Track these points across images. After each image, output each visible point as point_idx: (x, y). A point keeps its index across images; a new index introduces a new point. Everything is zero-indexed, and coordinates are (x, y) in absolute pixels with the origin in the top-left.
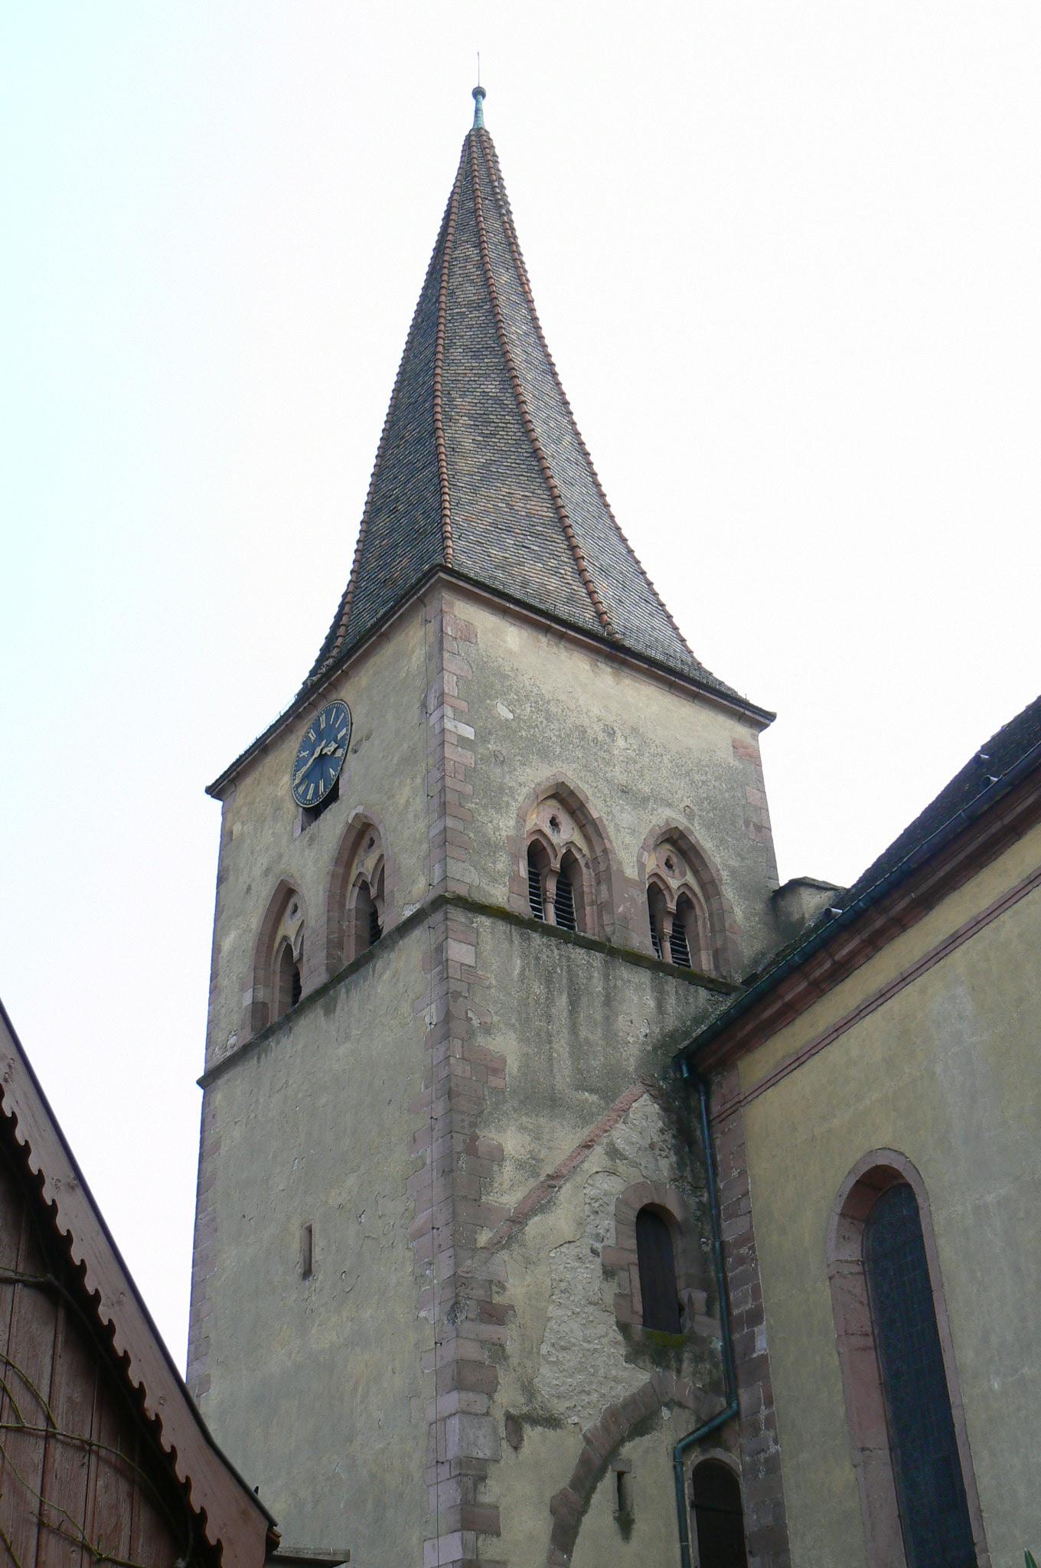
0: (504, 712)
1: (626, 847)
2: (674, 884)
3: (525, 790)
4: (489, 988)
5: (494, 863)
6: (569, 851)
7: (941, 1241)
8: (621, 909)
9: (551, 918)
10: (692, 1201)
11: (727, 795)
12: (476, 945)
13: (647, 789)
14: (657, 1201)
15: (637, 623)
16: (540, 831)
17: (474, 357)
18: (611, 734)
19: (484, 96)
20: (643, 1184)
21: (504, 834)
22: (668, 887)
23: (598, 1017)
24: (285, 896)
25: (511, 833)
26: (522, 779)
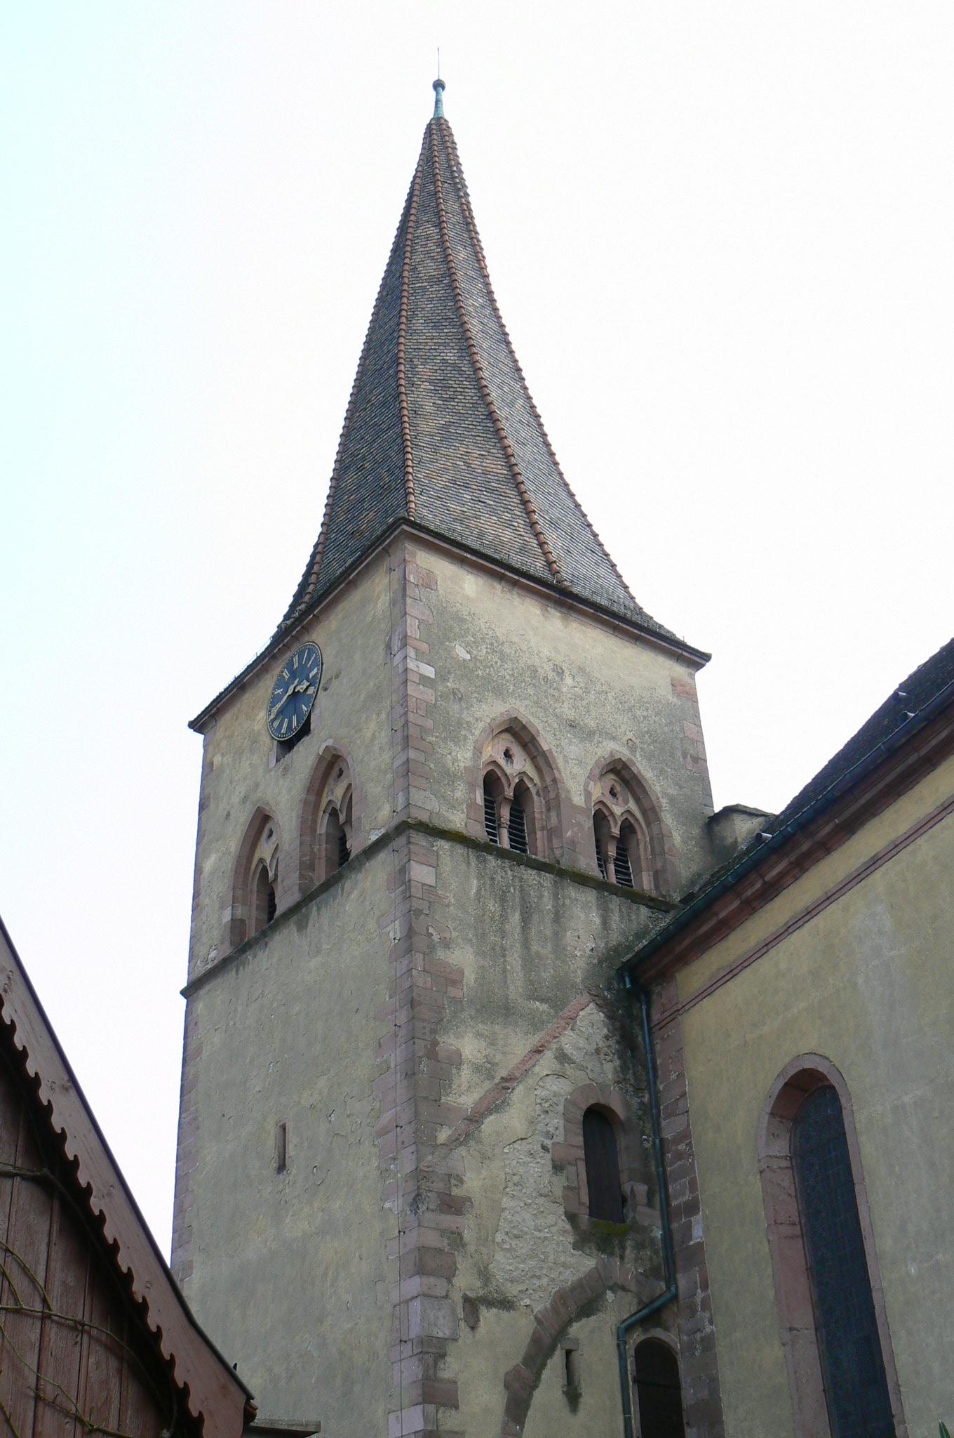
0: (462, 653)
1: (574, 777)
2: (618, 810)
3: (481, 725)
4: (448, 906)
5: (453, 791)
6: (521, 781)
7: (863, 1138)
8: (569, 834)
9: (505, 842)
10: (635, 1102)
11: (666, 729)
12: (436, 867)
13: (593, 724)
14: (602, 1101)
15: (584, 571)
16: (495, 762)
17: (435, 327)
18: (560, 673)
19: (443, 88)
20: (589, 1086)
21: (462, 764)
22: (612, 814)
23: (548, 933)
24: (262, 821)
25: (469, 764)
26: (478, 715)
